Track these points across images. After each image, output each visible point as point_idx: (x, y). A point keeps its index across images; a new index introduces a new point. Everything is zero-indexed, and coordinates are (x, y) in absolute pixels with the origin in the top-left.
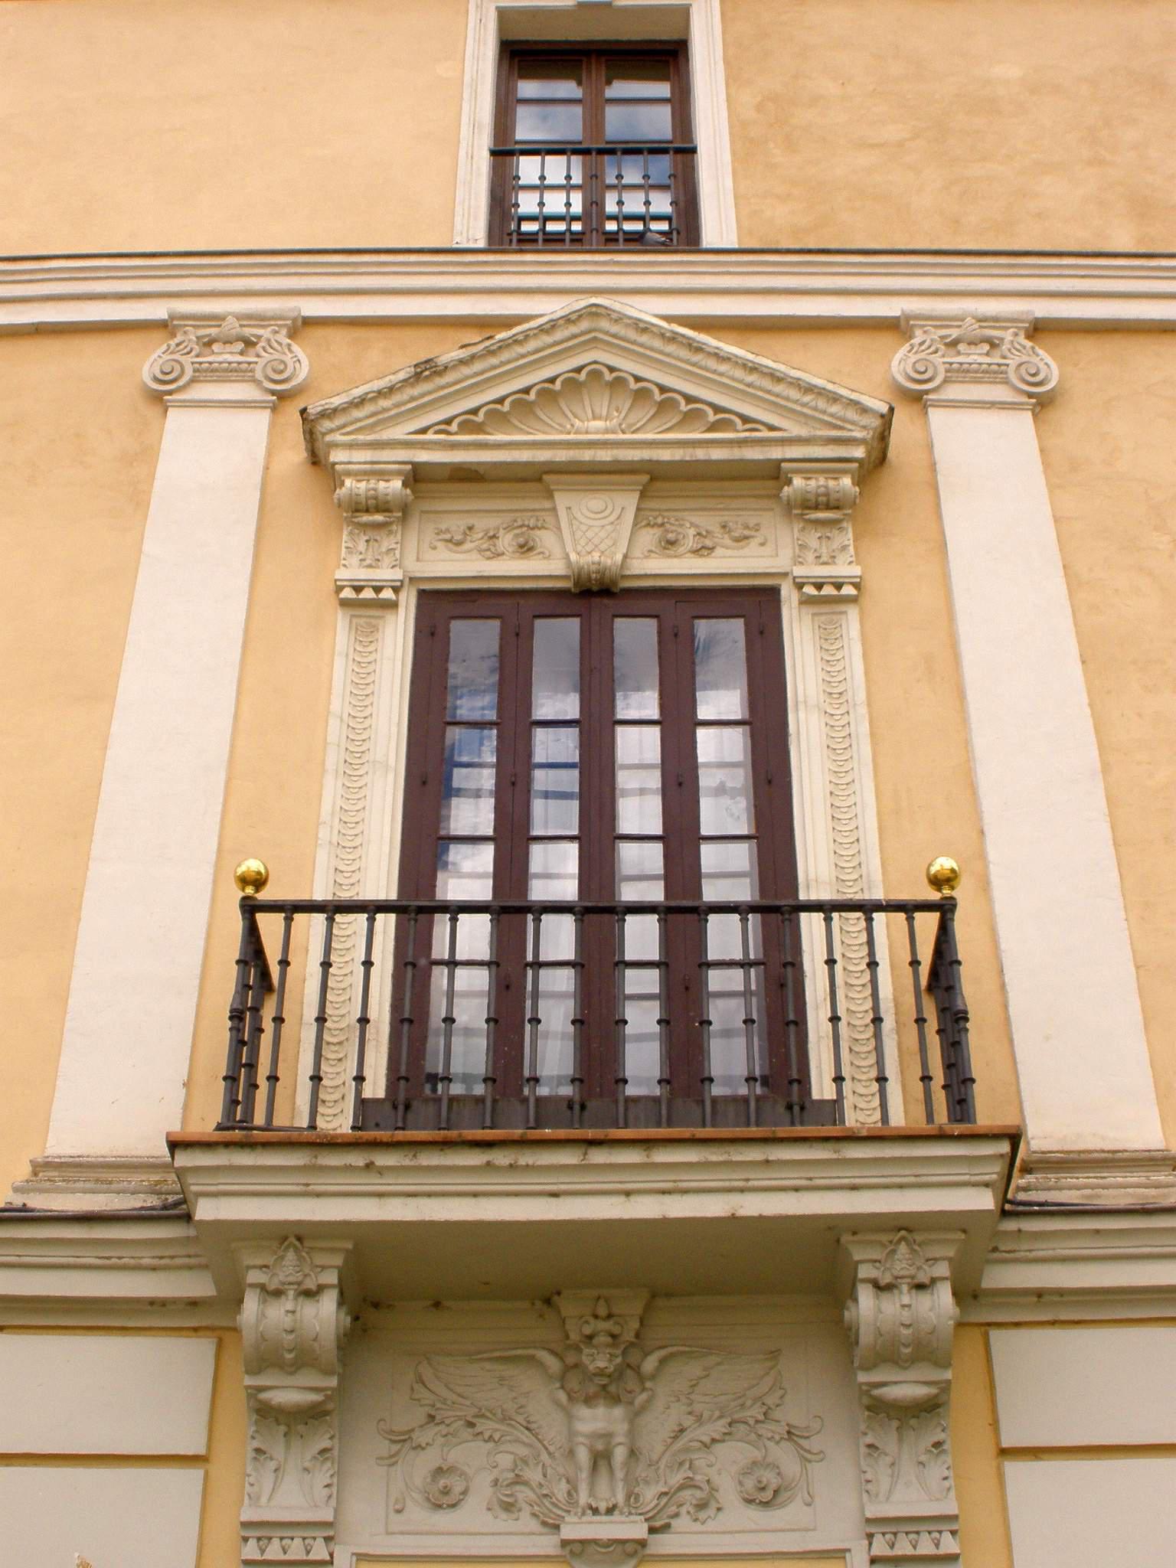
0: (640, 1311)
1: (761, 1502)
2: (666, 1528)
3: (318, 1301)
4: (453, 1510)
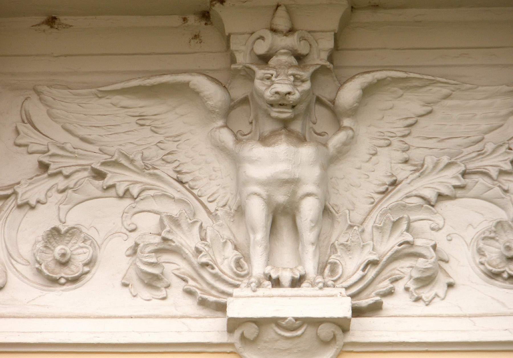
0: (334, 25)
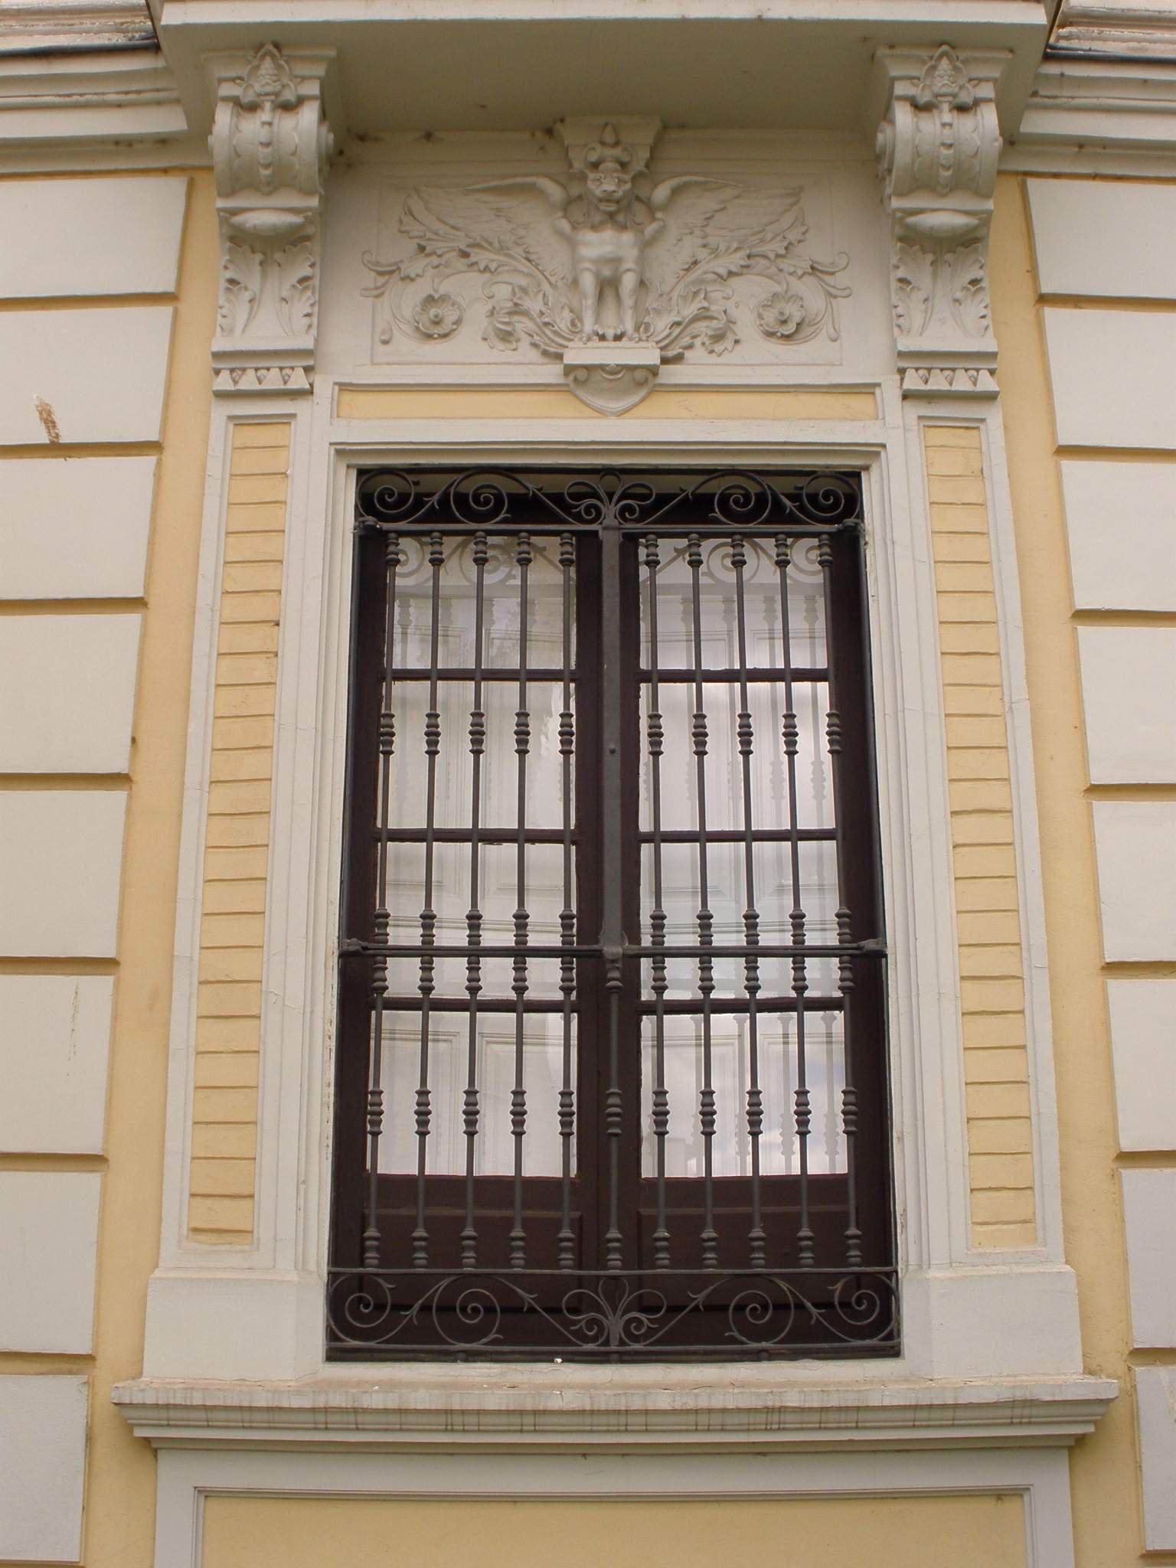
0: (650, 141)
1: (783, 336)
2: (678, 359)
3: (298, 113)
4: (444, 340)
